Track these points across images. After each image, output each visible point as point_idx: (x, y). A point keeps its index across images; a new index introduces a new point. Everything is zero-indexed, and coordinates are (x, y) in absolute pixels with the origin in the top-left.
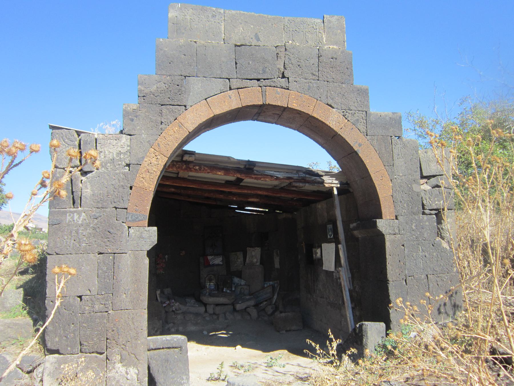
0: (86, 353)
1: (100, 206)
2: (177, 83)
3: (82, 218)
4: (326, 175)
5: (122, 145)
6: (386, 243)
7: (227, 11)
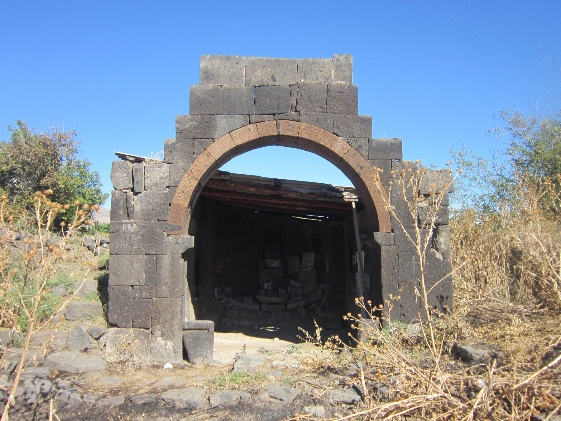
0: (136, 328)
1: (147, 218)
3: (133, 227)
4: (345, 191)
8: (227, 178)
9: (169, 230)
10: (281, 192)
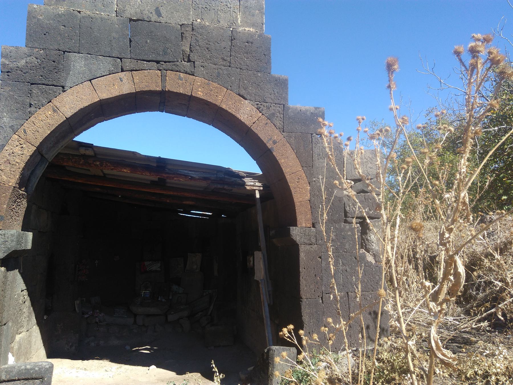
2: (52, 59)
4: (247, 177)
8: (89, 152)
10: (165, 176)
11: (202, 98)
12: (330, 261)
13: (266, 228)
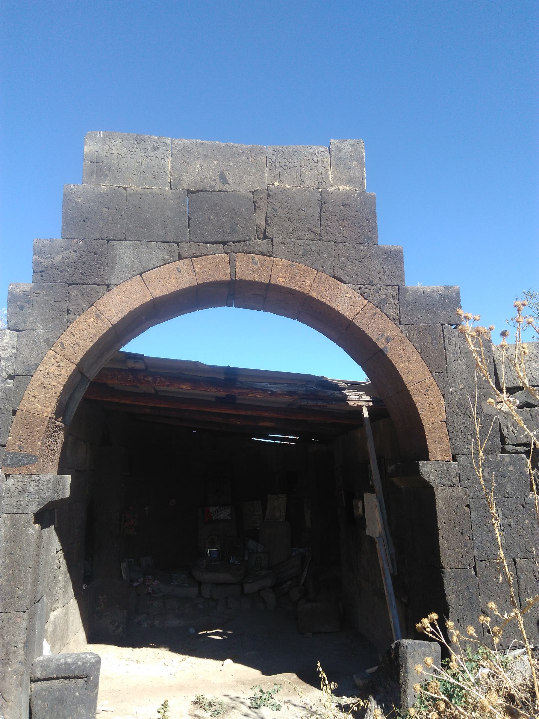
4: (349, 388)
5: (3, 347)
6: (437, 502)
7: (177, 141)
8: (139, 365)
9: (8, 465)
11: (284, 285)
12: (493, 524)
13: (380, 459)
